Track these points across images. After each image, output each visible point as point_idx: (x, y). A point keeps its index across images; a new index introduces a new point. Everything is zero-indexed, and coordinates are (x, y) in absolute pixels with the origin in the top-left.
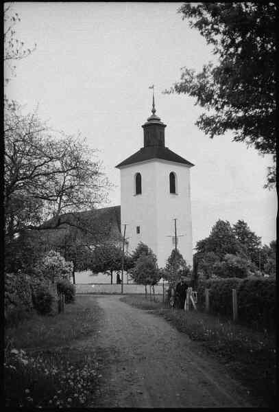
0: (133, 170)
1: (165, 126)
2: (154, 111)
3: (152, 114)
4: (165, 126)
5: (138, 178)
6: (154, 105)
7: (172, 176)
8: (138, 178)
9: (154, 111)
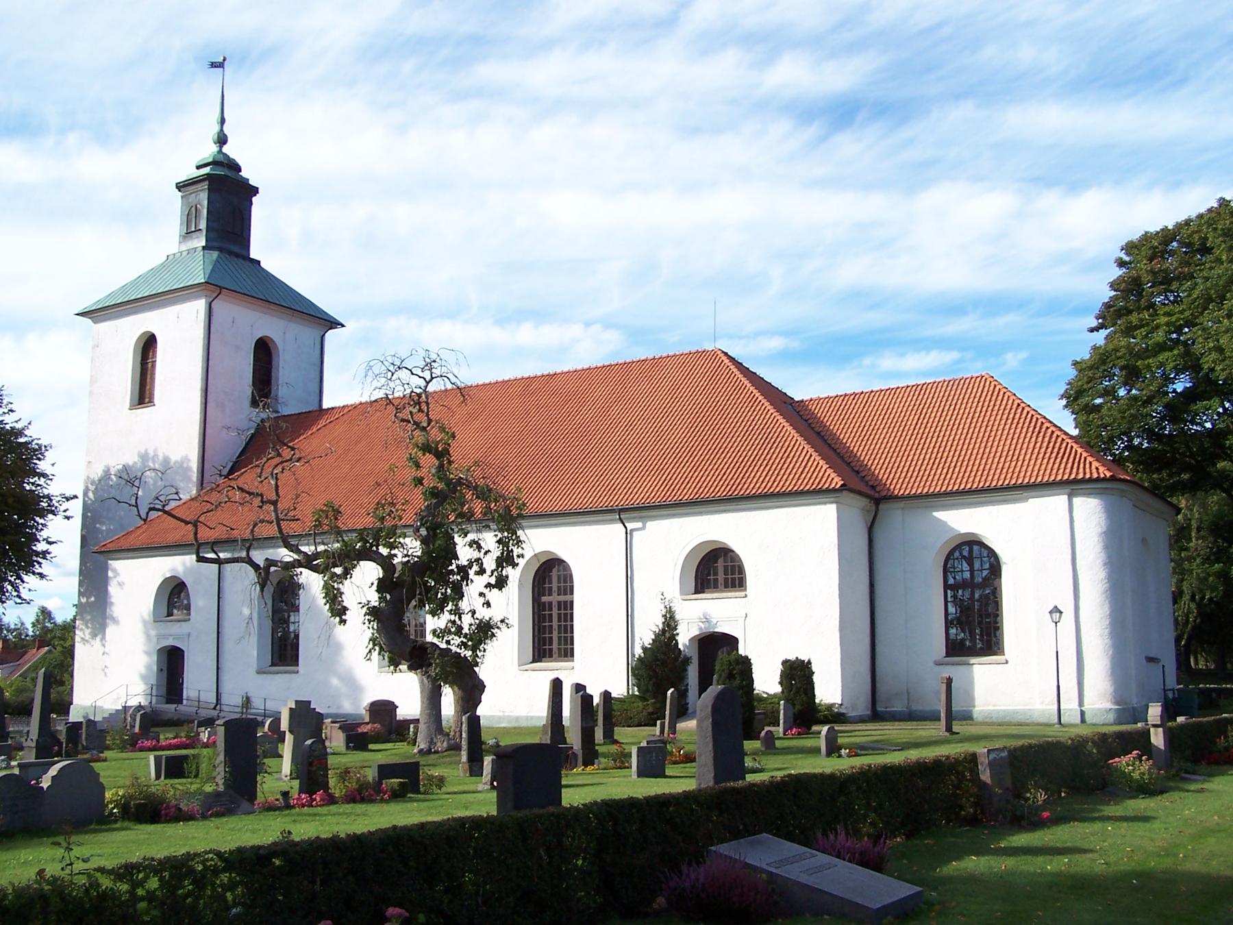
0: (132, 327)
1: (255, 191)
2: (222, 140)
3: (215, 148)
4: (255, 191)
5: (148, 344)
6: (223, 121)
7: (264, 351)
8: (148, 344)
9: (222, 140)
